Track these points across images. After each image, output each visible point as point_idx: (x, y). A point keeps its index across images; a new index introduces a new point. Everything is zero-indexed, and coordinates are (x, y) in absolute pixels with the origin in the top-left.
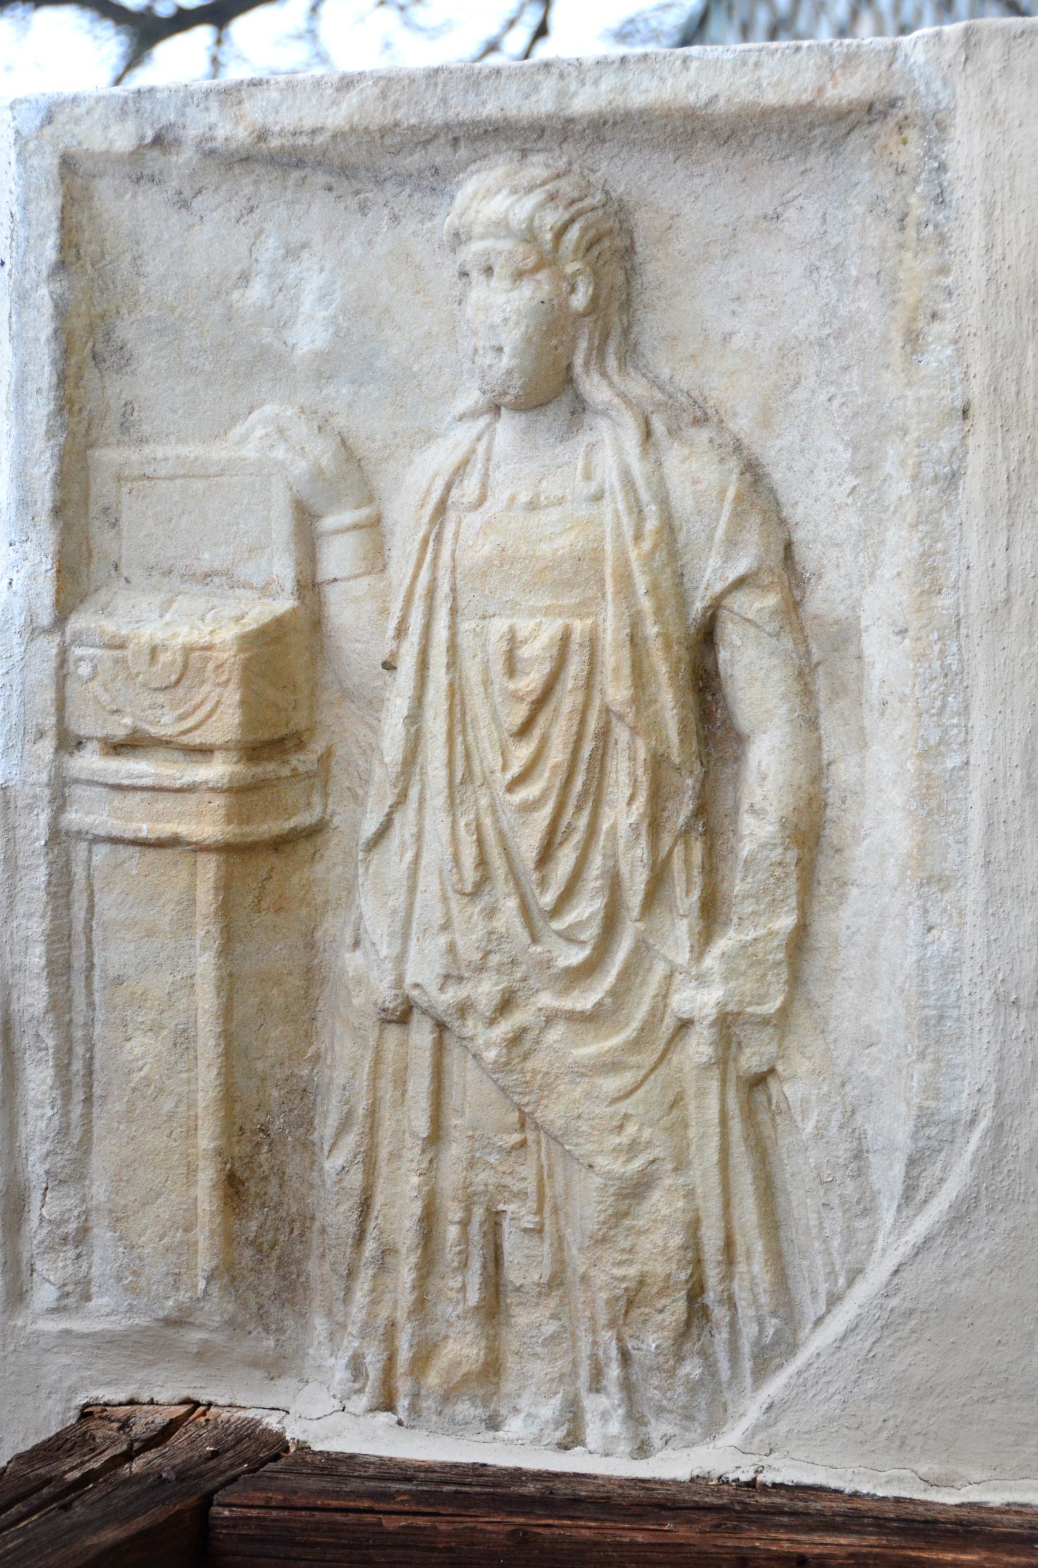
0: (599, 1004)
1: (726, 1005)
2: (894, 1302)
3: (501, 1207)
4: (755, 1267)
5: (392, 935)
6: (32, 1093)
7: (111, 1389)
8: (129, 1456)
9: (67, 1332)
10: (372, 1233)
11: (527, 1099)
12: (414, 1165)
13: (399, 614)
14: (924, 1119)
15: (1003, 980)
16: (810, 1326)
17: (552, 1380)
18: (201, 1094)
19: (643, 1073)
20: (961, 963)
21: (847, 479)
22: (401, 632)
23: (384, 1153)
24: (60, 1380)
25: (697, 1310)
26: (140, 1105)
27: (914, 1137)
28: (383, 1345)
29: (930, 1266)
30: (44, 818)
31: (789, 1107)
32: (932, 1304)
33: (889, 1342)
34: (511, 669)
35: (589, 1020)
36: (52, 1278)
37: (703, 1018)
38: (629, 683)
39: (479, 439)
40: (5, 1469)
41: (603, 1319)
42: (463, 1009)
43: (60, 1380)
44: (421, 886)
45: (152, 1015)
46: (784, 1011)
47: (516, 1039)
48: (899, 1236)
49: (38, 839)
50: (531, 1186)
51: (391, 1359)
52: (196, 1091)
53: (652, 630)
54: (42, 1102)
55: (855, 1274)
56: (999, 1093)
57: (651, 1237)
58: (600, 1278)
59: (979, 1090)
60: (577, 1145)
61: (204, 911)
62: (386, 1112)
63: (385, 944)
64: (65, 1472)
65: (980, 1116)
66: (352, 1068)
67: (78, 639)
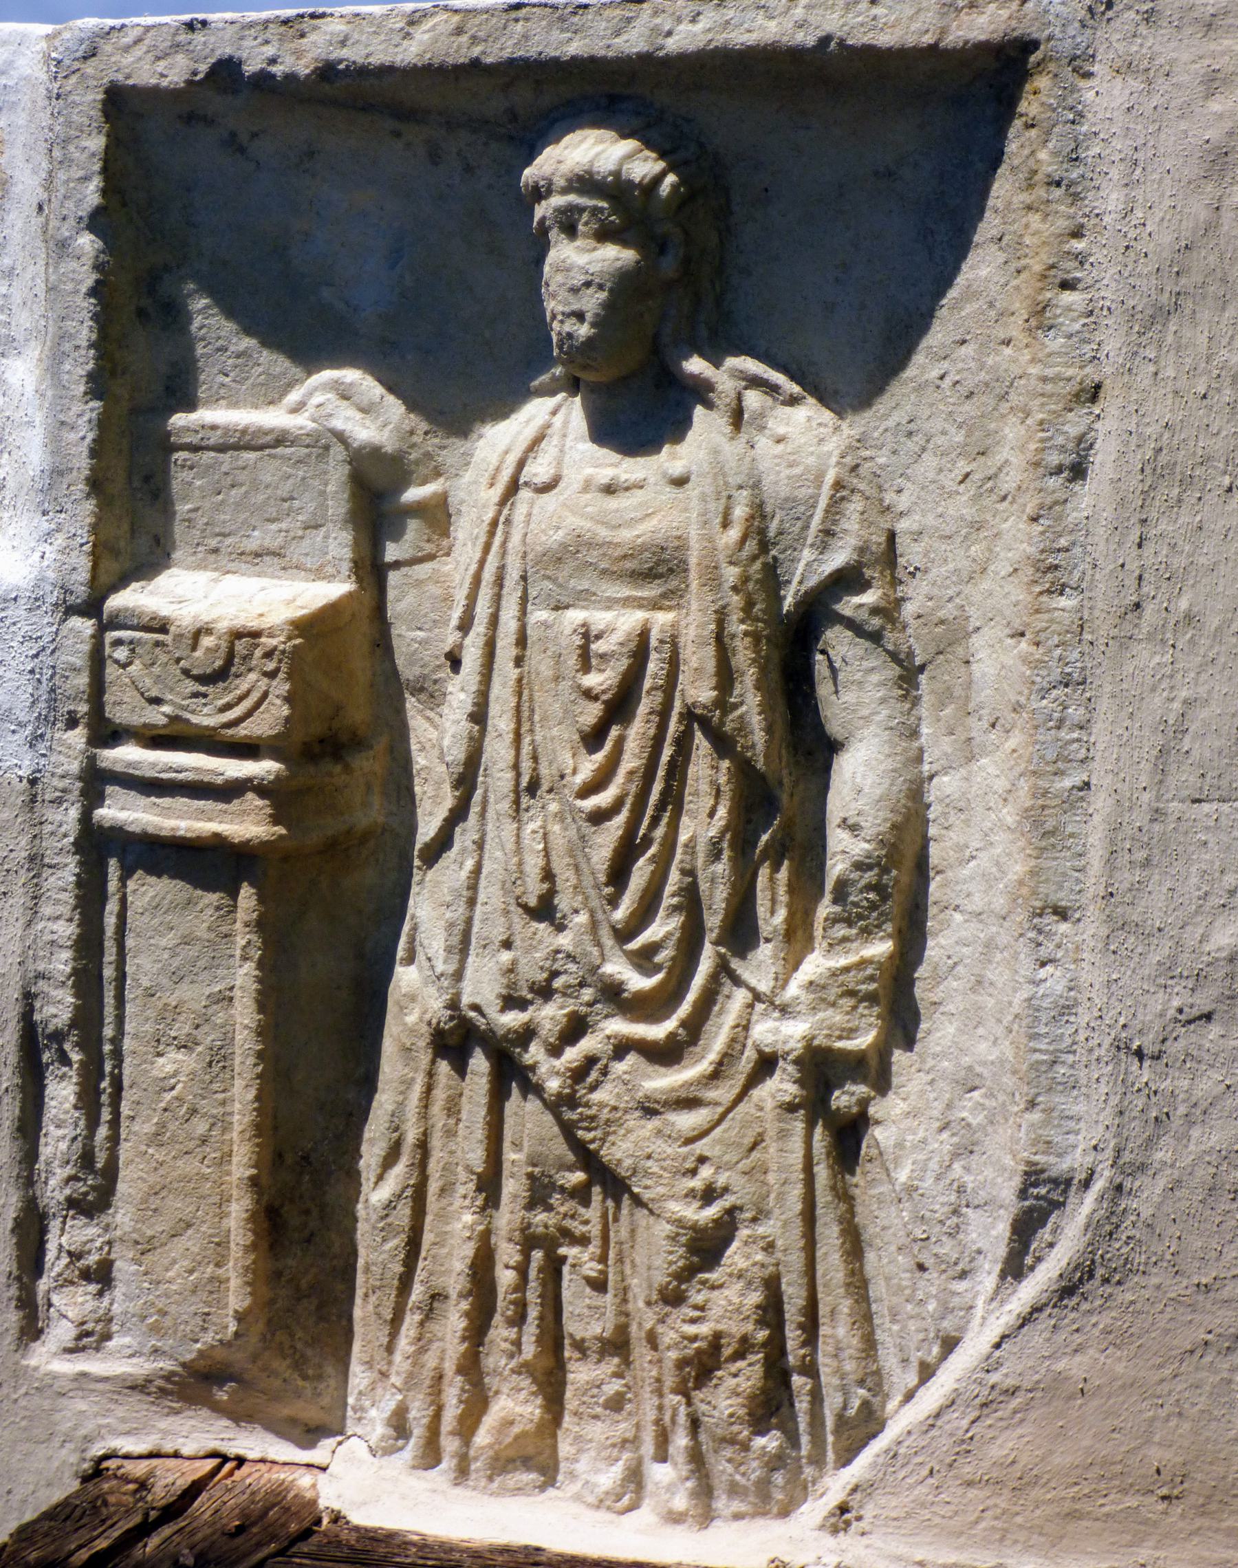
0: (672, 1036)
1: (814, 1038)
2: (994, 1378)
3: (562, 1251)
4: (838, 1331)
5: (449, 950)
6: (54, 1111)
7: (131, 1439)
8: (144, 1530)
9: (84, 1375)
10: (420, 1275)
11: (590, 1135)
12: (467, 1202)
13: (464, 602)
14: (1033, 1176)
15: (1124, 1026)
16: (899, 1398)
17: (614, 1445)
18: (237, 1117)
19: (720, 1110)
20: (1076, 1003)
21: (959, 465)
22: (465, 626)
23: (433, 1187)
24: (76, 1427)
25: (777, 1373)
26: (172, 1126)
27: (1023, 1194)
28: (429, 1399)
29: (1036, 1336)
30: (74, 813)
31: (881, 1154)
32: (1038, 1382)
33: (989, 1422)
34: (586, 661)
35: (665, 1054)
36: (70, 1314)
37: (788, 1054)
38: (713, 681)
39: (554, 413)
40: (5, 1545)
41: (669, 1381)
42: (527, 1034)
43: (76, 1427)
44: (482, 897)
45: (187, 1029)
46: (883, 1052)
47: (579, 1074)
48: (1002, 1302)
49: (65, 836)
50: (595, 1230)
51: (437, 1417)
52: (231, 1114)
53: (737, 627)
54: (64, 1121)
55: (950, 1344)
56: (1118, 1152)
57: (726, 1292)
58: (668, 1336)
59: (1095, 1148)
60: (646, 1187)
61: (247, 918)
62: (436, 1142)
63: (441, 960)
64: (71, 1554)
65: (1096, 1176)
66: (401, 1093)
67: (115, 622)
